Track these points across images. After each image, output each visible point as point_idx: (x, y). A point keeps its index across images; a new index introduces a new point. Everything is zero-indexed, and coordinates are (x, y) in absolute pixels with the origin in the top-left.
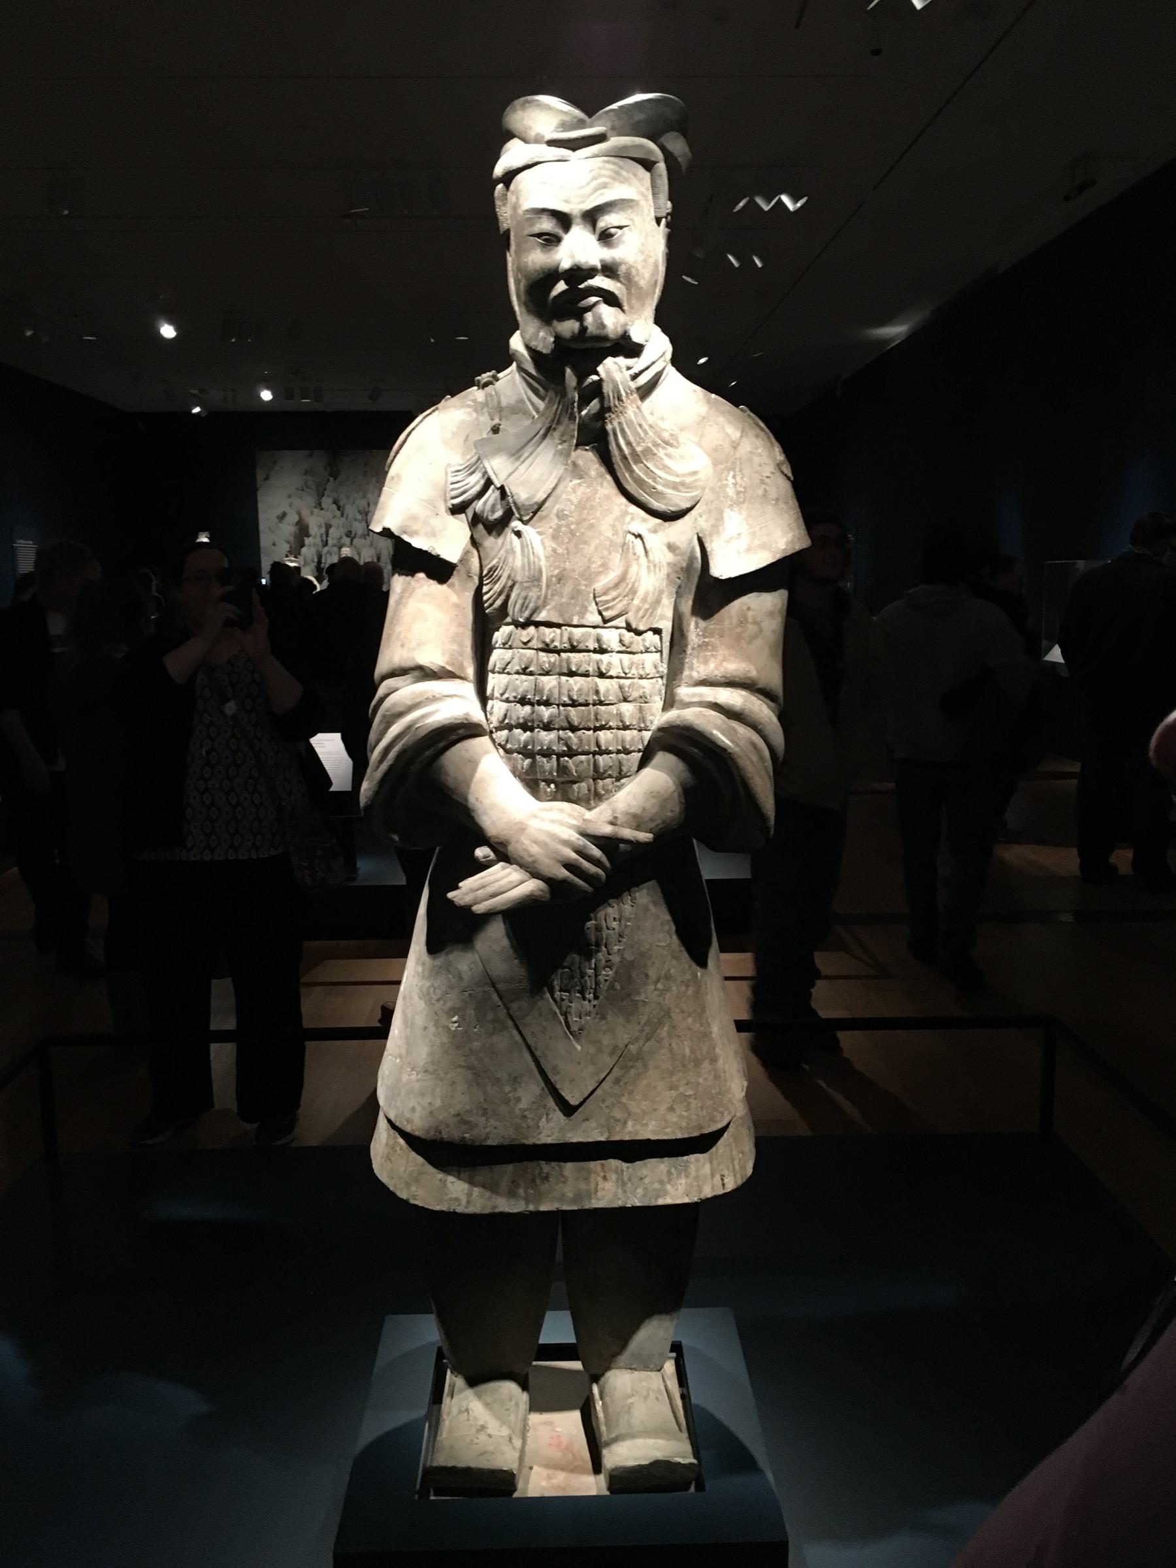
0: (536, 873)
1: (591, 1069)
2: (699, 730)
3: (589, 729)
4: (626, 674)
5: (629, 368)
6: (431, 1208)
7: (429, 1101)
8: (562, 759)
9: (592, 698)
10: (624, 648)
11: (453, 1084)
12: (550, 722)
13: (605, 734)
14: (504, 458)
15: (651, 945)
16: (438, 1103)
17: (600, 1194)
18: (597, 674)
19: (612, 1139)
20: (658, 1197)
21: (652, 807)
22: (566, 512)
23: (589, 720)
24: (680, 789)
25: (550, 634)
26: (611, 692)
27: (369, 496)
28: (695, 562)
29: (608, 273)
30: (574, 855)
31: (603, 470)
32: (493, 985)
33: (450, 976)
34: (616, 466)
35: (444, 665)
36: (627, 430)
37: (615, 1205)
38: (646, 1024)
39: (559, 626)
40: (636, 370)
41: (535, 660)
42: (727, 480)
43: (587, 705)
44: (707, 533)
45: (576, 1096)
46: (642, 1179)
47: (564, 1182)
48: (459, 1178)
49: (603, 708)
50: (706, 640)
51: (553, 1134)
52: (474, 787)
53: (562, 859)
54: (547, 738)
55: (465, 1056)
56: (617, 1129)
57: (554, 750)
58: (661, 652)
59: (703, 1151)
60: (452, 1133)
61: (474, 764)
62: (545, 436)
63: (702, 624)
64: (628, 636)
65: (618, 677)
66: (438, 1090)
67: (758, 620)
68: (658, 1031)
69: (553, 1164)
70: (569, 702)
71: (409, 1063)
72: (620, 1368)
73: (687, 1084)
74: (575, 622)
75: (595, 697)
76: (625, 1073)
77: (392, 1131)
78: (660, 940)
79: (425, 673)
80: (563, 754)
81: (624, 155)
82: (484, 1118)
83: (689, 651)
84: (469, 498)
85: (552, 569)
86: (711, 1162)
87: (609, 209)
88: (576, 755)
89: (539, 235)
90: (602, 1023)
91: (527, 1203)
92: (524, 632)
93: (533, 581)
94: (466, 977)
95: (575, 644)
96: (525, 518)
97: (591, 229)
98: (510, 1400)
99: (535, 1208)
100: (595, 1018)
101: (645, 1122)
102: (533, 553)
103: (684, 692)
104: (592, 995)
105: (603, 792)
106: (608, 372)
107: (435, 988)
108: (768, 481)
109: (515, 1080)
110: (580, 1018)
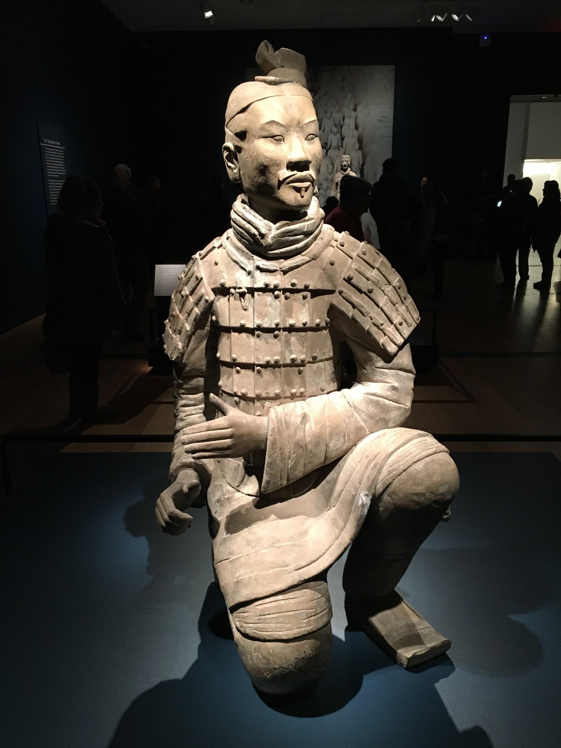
27: (345, 110)
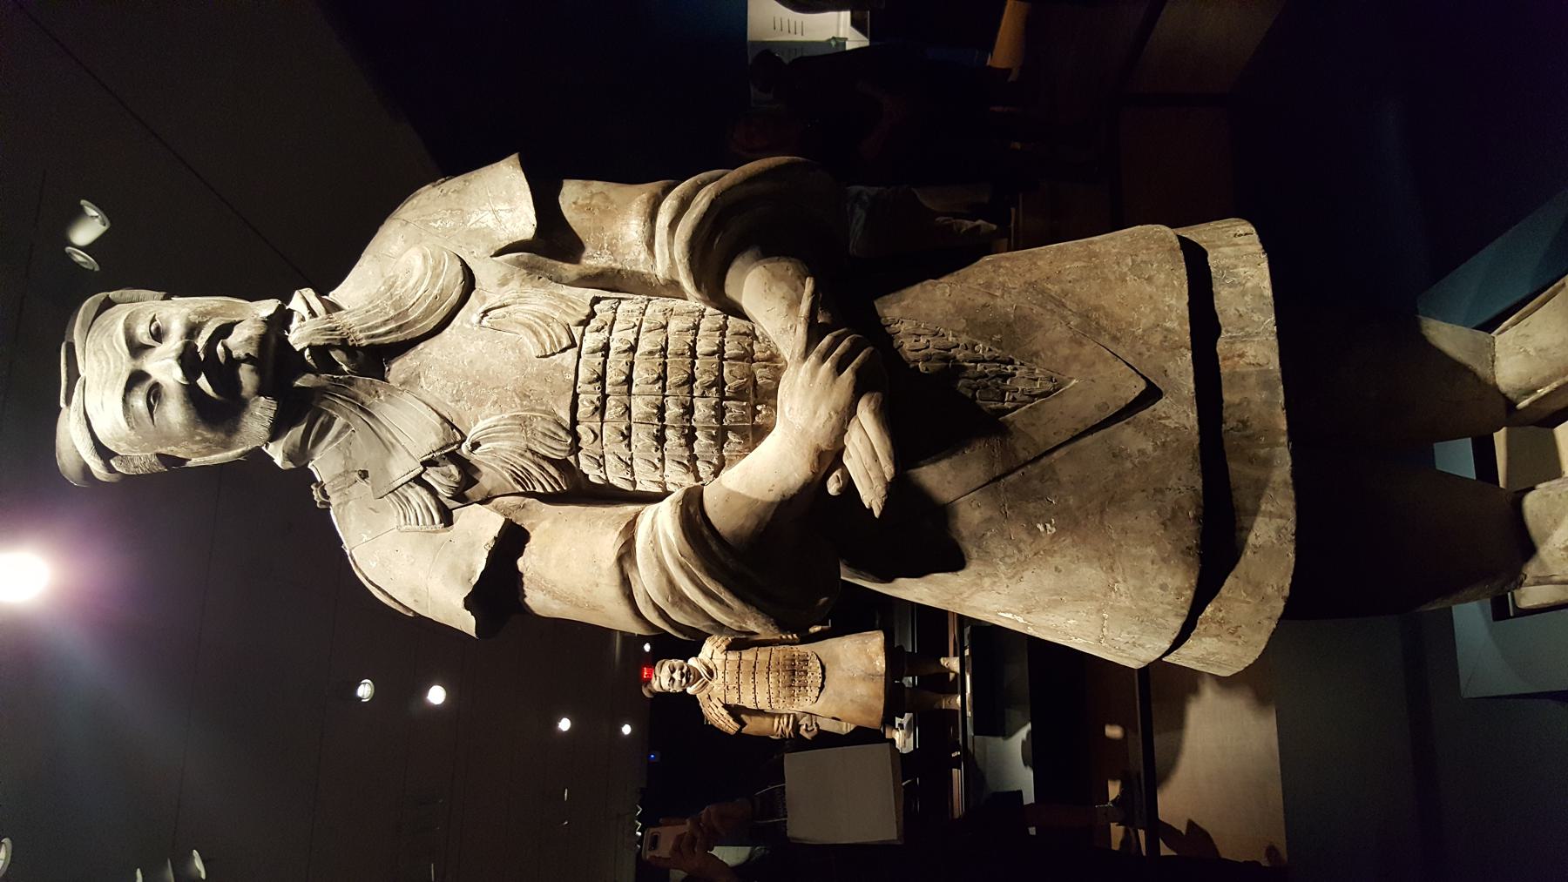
0: (849, 408)
1: (1100, 366)
2: (691, 233)
3: (693, 364)
4: (635, 325)
5: (303, 319)
6: (1293, 566)
7: (1149, 563)
8: (727, 394)
9: (658, 359)
10: (607, 328)
11: (1124, 531)
12: (684, 406)
13: (700, 347)
14: (392, 462)
15: (948, 301)
16: (1151, 551)
17: (1262, 361)
18: (631, 354)
19: (1189, 344)
20: (1262, 296)
21: (782, 289)
22: (455, 392)
23: (683, 362)
24: (762, 261)
25: (585, 406)
26: (654, 339)
28: (522, 259)
29: (196, 333)
30: (828, 364)
31: (412, 353)
32: (997, 479)
33: (989, 534)
34: (409, 337)
35: (618, 533)
36: (369, 324)
37: (1276, 343)
38: (1045, 308)
39: (576, 396)
40: (305, 312)
41: (613, 424)
42: (437, 228)
43: (665, 364)
44: (490, 246)
45: (1134, 382)
46: (1240, 315)
47: (1249, 402)
48: (1249, 529)
49: (670, 348)
50: (606, 245)
51: (1185, 411)
52: (755, 496)
53: (831, 377)
54: (702, 410)
55: (1088, 514)
56: (1177, 339)
57: (716, 403)
58: (620, 299)
59: (1205, 254)
60: (1189, 533)
61: (730, 495)
62: (370, 414)
63: (589, 251)
64: (594, 323)
65: (638, 334)
66: (1133, 551)
67: (588, 195)
68: (1053, 294)
69: (1225, 415)
70: (660, 384)
71: (1105, 595)
72: (1493, 373)
73: (1118, 264)
74: (572, 377)
75: (657, 356)
76: (1105, 331)
77: (1200, 627)
78: (944, 294)
79: (626, 553)
80: (721, 392)
81: (90, 323)
82: (1167, 492)
83: (618, 266)
84: (433, 502)
85: (514, 405)
86: (1220, 247)
87: (132, 331)
88: (723, 378)
89: (150, 408)
90: (1043, 356)
91: (1278, 444)
92: (584, 438)
93: (526, 426)
94: (989, 513)
95: (595, 376)
96: (459, 438)
97: (150, 350)
98: (1548, 496)
99: (1284, 435)
100: (1037, 364)
101: (1166, 308)
102: (495, 426)
103: (661, 270)
104: (1008, 367)
105: (768, 352)
106: (301, 339)
107: (1006, 556)
108: (445, 191)
109: (1117, 455)
110: (1036, 380)
